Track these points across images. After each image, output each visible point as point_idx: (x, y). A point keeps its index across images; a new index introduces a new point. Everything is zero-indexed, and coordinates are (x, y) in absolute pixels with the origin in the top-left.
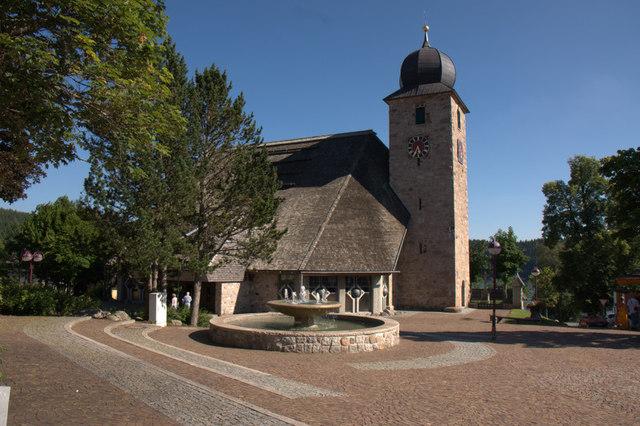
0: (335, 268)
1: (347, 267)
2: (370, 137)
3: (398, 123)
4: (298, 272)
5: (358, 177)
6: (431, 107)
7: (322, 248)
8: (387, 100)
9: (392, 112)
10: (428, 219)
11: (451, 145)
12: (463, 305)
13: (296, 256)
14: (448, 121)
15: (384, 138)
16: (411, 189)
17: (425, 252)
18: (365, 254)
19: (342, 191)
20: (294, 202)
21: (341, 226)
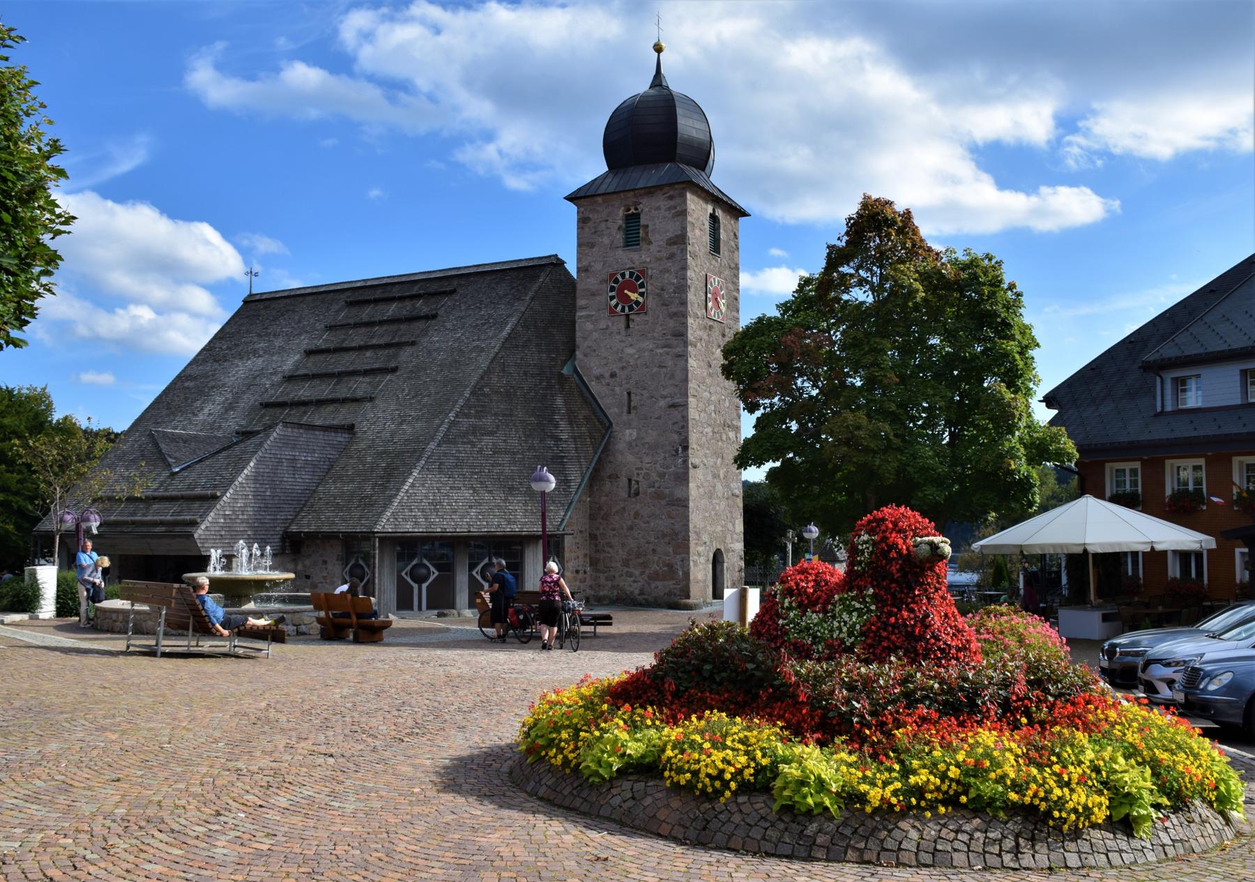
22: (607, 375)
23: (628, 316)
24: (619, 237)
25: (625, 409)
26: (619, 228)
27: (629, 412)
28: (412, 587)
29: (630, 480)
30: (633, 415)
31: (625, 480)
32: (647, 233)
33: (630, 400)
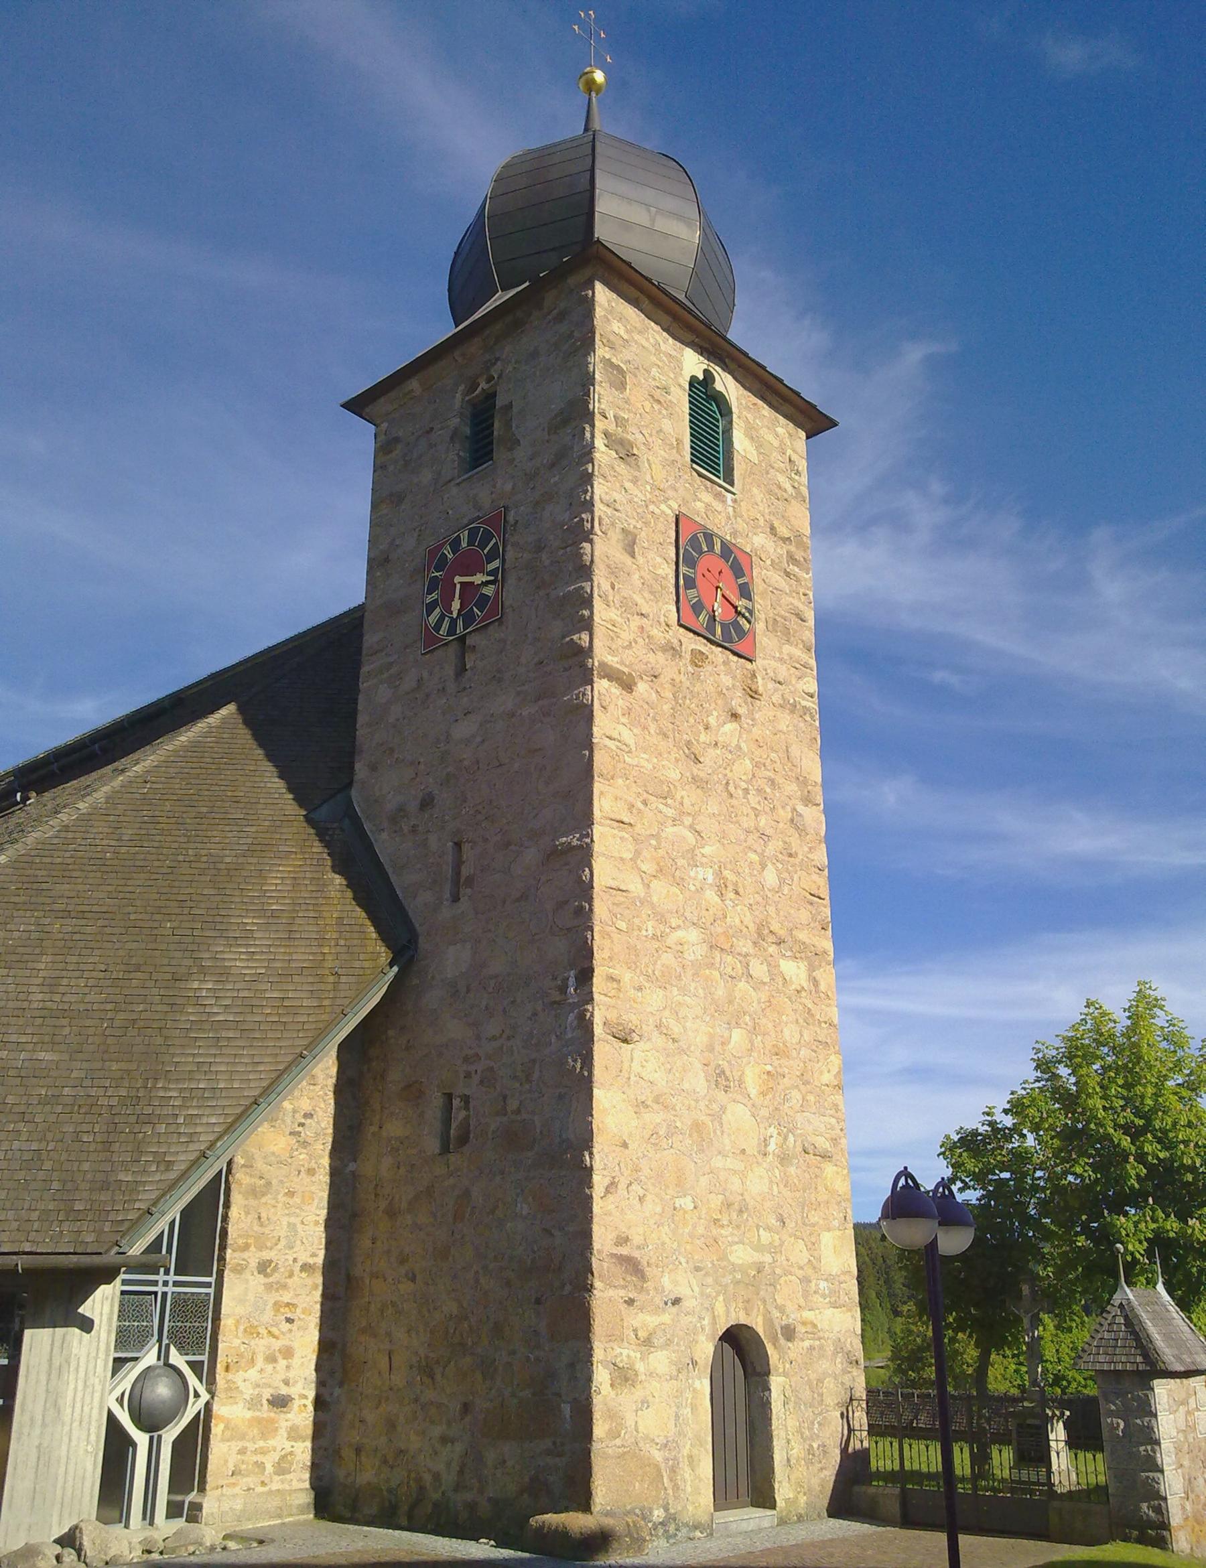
8: (357, 406)
16: (427, 803)
22: (413, 807)
23: (462, 639)
24: (451, 457)
25: (447, 888)
26: (455, 435)
27: (456, 899)
28: (176, 1444)
29: (449, 1097)
30: (464, 904)
31: (437, 1101)
32: (508, 425)
33: (458, 864)
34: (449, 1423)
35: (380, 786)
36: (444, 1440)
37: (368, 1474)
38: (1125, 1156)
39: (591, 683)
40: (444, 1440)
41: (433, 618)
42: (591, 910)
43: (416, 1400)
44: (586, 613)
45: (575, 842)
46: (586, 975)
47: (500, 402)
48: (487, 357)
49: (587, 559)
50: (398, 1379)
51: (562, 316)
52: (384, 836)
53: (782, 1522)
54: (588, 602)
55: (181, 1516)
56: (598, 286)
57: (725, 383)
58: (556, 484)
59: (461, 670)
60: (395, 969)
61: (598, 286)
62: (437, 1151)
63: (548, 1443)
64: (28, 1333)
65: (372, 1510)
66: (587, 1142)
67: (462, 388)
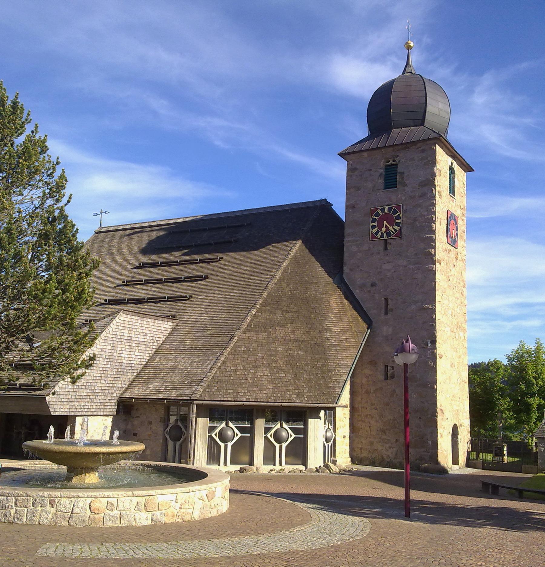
0: (246, 397)
1: (265, 395)
2: (324, 207)
3: (359, 189)
4: (189, 402)
5: (305, 242)
6: (406, 163)
7: (230, 367)
8: (343, 155)
9: (351, 171)
10: (401, 315)
11: (432, 221)
12: (455, 461)
13: (191, 378)
14: (429, 183)
15: (340, 208)
16: (373, 285)
17: (393, 377)
18: (295, 377)
19: (271, 286)
20: (203, 300)
21: (263, 336)
23: (386, 240)
29: (386, 366)
30: (389, 315)
31: (382, 367)
32: (403, 178)
33: (387, 304)
34: (392, 444)
35: (354, 276)
36: (390, 448)
37: (365, 454)
38: (533, 385)
39: (435, 264)
40: (390, 448)
41: (375, 230)
42: (436, 325)
43: (380, 438)
44: (434, 244)
45: (430, 307)
46: (434, 342)
47: (399, 170)
48: (394, 154)
49: (434, 228)
50: (373, 433)
51: (423, 151)
52: (357, 291)
53: (460, 468)
54: (434, 241)
55: (353, 462)
56: (437, 146)
57: (456, 166)
58: (422, 202)
59: (386, 248)
60: (369, 330)
61: (437, 146)
62: (383, 379)
63: (425, 450)
64: (309, 420)
65: (367, 462)
66: (435, 382)
67: (383, 160)
